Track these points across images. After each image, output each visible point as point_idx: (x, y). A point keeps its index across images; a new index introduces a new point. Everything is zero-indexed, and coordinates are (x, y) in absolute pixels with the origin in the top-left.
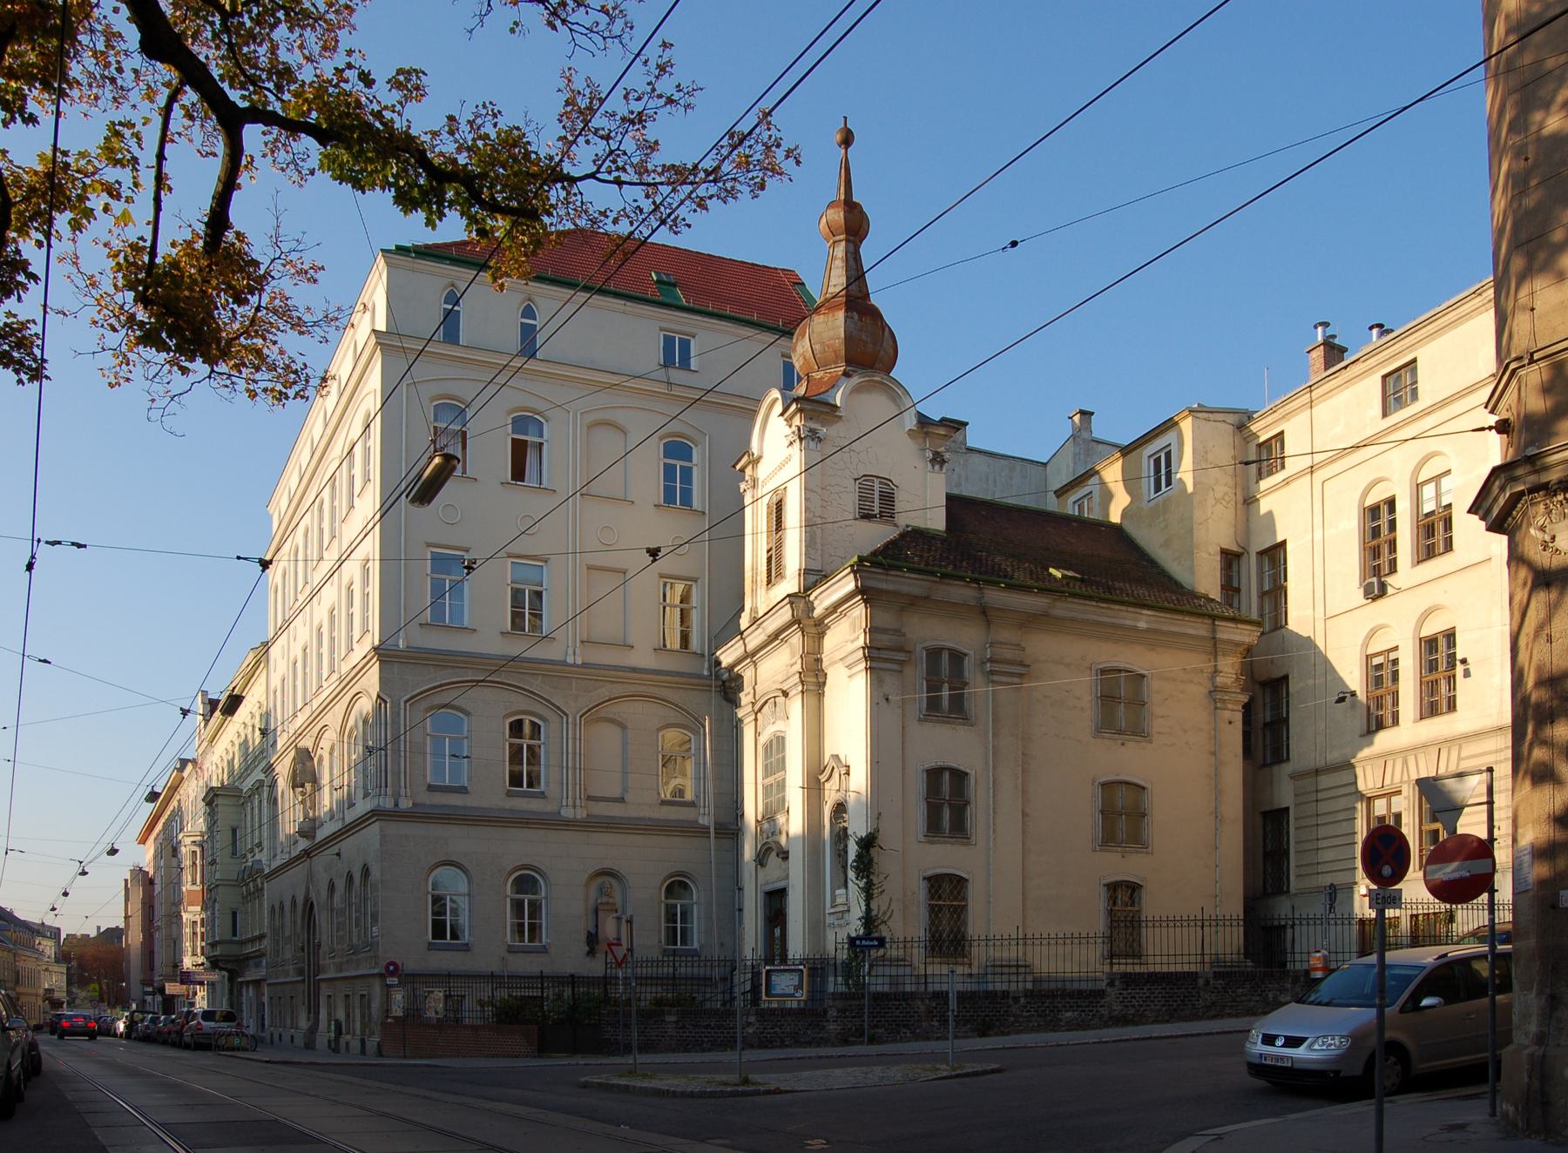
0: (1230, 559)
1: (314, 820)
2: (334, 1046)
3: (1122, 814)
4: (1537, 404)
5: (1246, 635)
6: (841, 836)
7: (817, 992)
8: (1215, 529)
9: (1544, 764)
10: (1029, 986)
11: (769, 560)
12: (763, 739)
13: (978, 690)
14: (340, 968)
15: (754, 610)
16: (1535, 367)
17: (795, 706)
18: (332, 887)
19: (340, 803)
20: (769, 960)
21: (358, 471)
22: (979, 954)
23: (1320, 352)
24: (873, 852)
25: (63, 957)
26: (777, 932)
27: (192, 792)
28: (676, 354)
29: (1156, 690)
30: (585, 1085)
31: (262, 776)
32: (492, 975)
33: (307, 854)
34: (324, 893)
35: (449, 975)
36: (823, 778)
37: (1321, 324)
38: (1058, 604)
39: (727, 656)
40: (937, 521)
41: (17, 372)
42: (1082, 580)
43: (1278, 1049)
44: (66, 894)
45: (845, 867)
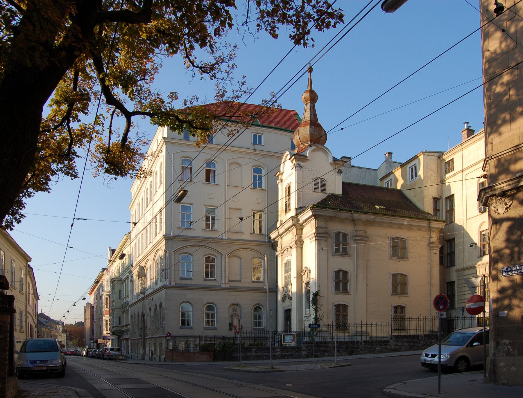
0: (436, 200)
1: (145, 288)
2: (151, 359)
3: (399, 284)
4: (493, 171)
5: (440, 225)
6: (308, 292)
7: (299, 342)
8: (431, 192)
9: (495, 275)
10: (368, 339)
11: (286, 205)
12: (284, 262)
13: (352, 246)
14: (153, 334)
15: (282, 221)
16: (493, 160)
17: (294, 251)
18: (150, 309)
19: (153, 283)
20: (286, 331)
21: (158, 180)
22: (352, 329)
23: (466, 132)
24: (318, 297)
25: (65, 331)
26: (288, 322)
27: (106, 279)
28: (257, 140)
29: (410, 244)
30: (225, 370)
31: (129, 274)
32: (199, 337)
33: (143, 299)
34: (148, 311)
35: (186, 337)
36: (302, 274)
37: (466, 123)
38: (378, 217)
39: (273, 235)
40: (339, 191)
41: (71, 176)
42: (386, 209)
43: (429, 358)
44: (68, 312)
45: (309, 302)
